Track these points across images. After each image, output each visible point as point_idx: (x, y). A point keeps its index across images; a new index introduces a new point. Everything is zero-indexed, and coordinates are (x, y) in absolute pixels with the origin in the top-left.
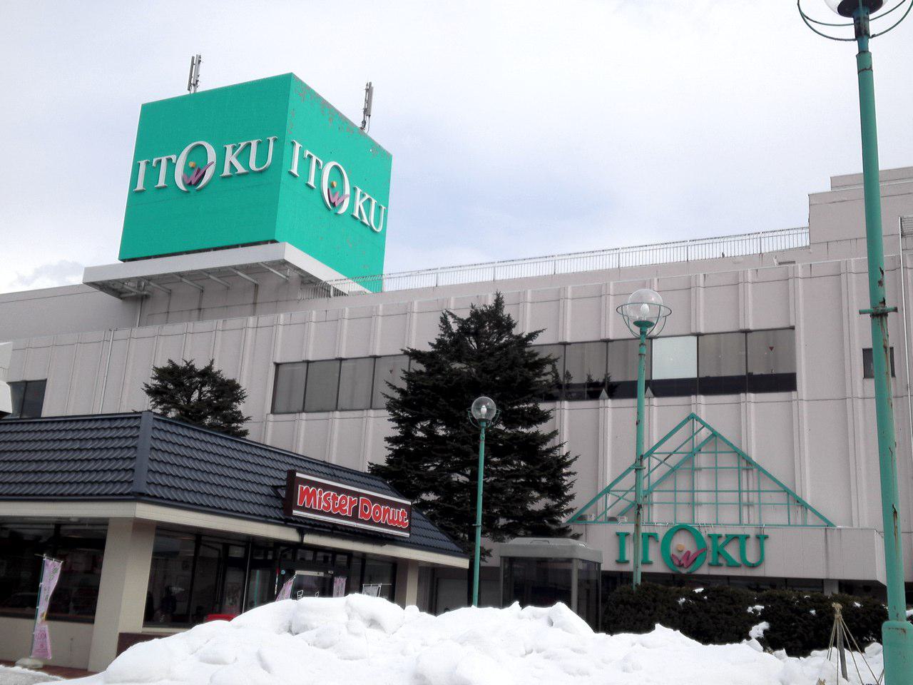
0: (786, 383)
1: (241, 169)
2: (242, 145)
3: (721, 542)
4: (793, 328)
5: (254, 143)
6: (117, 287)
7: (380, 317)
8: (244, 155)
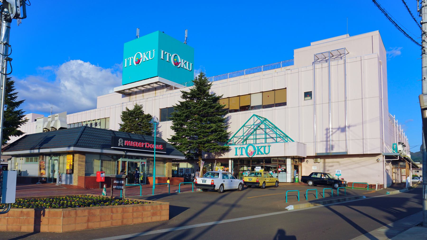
0: (285, 104)
1: (147, 59)
2: (147, 52)
3: (260, 148)
4: (286, 88)
5: (150, 52)
6: (186, 63)
7: (154, 100)
8: (147, 56)
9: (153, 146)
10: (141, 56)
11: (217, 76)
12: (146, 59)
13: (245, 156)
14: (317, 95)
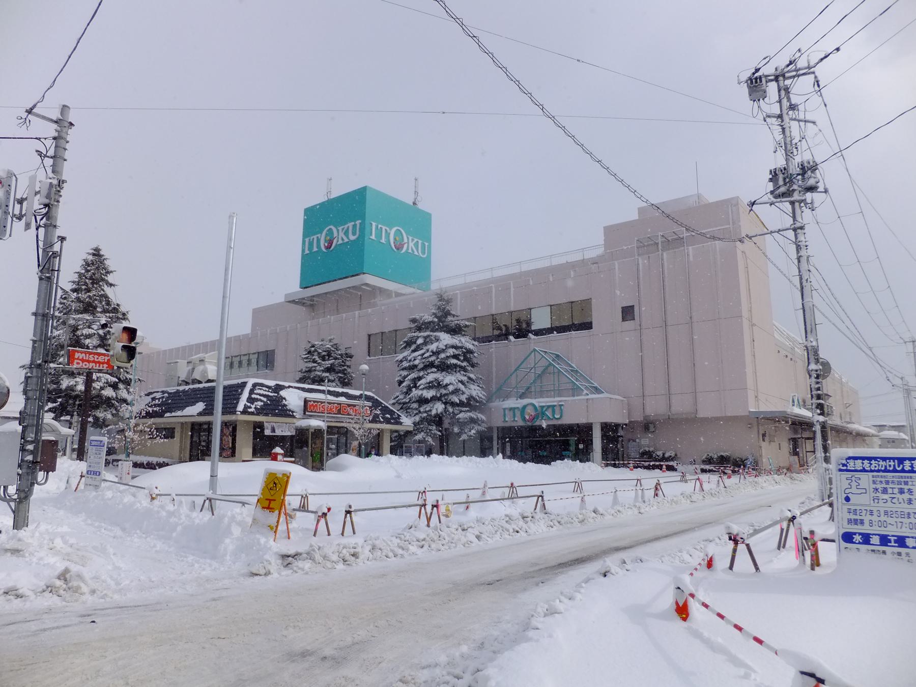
0: (587, 326)
1: (346, 240)
9: (367, 406)
10: (335, 234)
11: (224, 594)
12: (343, 239)
13: (521, 423)
14: (644, 312)
